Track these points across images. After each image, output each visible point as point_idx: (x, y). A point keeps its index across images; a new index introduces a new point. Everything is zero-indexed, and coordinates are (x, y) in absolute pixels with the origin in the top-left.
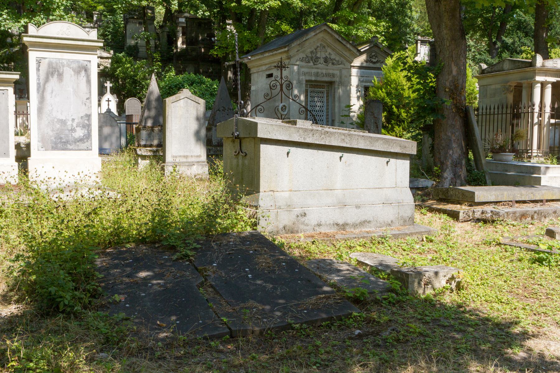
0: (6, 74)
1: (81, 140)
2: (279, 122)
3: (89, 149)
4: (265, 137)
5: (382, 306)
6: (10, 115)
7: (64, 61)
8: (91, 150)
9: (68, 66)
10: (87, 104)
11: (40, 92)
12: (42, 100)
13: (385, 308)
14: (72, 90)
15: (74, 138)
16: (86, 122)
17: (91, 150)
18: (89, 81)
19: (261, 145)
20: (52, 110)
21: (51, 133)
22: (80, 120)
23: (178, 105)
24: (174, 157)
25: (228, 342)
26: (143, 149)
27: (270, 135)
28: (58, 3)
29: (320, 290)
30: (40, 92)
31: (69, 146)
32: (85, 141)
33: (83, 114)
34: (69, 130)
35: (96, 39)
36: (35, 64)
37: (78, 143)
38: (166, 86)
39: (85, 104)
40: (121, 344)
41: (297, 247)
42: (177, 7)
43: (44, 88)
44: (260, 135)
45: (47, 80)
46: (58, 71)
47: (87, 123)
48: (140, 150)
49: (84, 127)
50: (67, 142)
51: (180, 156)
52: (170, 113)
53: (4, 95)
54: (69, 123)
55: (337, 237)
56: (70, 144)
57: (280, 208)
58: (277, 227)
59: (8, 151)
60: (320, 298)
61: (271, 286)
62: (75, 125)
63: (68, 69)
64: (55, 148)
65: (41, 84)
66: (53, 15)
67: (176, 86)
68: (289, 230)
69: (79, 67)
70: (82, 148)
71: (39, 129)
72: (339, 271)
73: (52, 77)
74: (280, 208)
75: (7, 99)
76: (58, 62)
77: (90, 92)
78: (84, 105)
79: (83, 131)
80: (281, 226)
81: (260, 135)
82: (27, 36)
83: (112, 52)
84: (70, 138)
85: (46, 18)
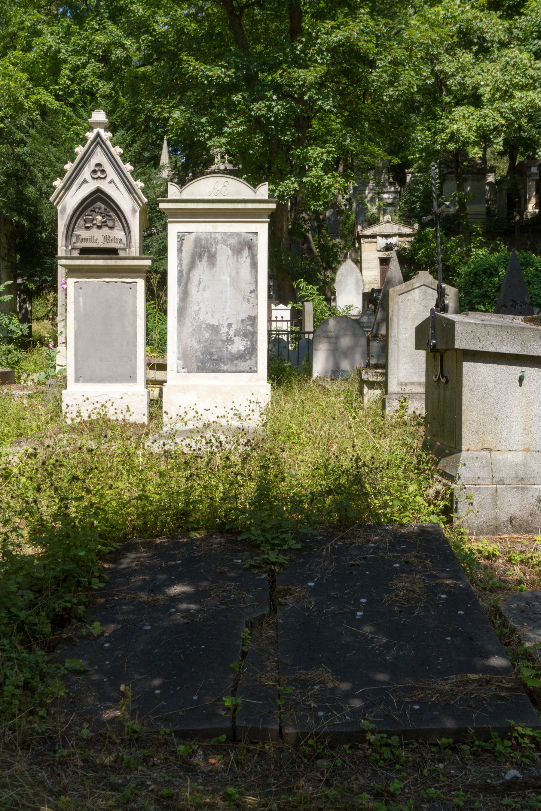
0: (111, 259)
1: (241, 356)
2: (518, 321)
3: (253, 370)
4: (471, 347)
6: (138, 320)
7: (217, 235)
8: (256, 372)
9: (224, 242)
10: (252, 300)
11: (182, 284)
12: (185, 295)
14: (229, 279)
15: (231, 353)
16: (249, 328)
17: (256, 372)
18: (254, 265)
19: (465, 364)
20: (199, 310)
21: (196, 346)
22: (240, 325)
23: (410, 297)
24: (401, 384)
25: (218, 749)
26: (371, 372)
27: (481, 345)
28: (315, 158)
29: (479, 662)
30: (182, 284)
31: (222, 365)
32: (247, 357)
33: (244, 316)
34: (223, 342)
35: (266, 198)
36: (176, 243)
37: (236, 362)
38: (470, 272)
39: (248, 301)
40: (290, 600)
41: (522, 561)
42: (502, 148)
43: (188, 278)
44: (460, 343)
45: (192, 265)
46: (209, 251)
47: (251, 329)
48: (366, 373)
49: (245, 335)
50: (220, 360)
51: (413, 383)
52: (395, 311)
53: (131, 291)
54: (224, 330)
56: (224, 363)
57: (501, 482)
58: (496, 518)
59: (135, 374)
60: (468, 682)
61: (385, 640)
62: (232, 333)
63: (224, 247)
64: (202, 369)
65: (184, 272)
66: (308, 177)
67: (484, 272)
68: (520, 527)
69: (240, 243)
70: (243, 369)
71: (179, 339)
73: (200, 261)
74: (501, 482)
75: (135, 297)
76: (209, 237)
77: (256, 282)
78: (246, 302)
79: (244, 343)
80: (504, 517)
81: (460, 343)
82: (164, 202)
83: (416, 226)
84: (225, 353)
85: (297, 181)
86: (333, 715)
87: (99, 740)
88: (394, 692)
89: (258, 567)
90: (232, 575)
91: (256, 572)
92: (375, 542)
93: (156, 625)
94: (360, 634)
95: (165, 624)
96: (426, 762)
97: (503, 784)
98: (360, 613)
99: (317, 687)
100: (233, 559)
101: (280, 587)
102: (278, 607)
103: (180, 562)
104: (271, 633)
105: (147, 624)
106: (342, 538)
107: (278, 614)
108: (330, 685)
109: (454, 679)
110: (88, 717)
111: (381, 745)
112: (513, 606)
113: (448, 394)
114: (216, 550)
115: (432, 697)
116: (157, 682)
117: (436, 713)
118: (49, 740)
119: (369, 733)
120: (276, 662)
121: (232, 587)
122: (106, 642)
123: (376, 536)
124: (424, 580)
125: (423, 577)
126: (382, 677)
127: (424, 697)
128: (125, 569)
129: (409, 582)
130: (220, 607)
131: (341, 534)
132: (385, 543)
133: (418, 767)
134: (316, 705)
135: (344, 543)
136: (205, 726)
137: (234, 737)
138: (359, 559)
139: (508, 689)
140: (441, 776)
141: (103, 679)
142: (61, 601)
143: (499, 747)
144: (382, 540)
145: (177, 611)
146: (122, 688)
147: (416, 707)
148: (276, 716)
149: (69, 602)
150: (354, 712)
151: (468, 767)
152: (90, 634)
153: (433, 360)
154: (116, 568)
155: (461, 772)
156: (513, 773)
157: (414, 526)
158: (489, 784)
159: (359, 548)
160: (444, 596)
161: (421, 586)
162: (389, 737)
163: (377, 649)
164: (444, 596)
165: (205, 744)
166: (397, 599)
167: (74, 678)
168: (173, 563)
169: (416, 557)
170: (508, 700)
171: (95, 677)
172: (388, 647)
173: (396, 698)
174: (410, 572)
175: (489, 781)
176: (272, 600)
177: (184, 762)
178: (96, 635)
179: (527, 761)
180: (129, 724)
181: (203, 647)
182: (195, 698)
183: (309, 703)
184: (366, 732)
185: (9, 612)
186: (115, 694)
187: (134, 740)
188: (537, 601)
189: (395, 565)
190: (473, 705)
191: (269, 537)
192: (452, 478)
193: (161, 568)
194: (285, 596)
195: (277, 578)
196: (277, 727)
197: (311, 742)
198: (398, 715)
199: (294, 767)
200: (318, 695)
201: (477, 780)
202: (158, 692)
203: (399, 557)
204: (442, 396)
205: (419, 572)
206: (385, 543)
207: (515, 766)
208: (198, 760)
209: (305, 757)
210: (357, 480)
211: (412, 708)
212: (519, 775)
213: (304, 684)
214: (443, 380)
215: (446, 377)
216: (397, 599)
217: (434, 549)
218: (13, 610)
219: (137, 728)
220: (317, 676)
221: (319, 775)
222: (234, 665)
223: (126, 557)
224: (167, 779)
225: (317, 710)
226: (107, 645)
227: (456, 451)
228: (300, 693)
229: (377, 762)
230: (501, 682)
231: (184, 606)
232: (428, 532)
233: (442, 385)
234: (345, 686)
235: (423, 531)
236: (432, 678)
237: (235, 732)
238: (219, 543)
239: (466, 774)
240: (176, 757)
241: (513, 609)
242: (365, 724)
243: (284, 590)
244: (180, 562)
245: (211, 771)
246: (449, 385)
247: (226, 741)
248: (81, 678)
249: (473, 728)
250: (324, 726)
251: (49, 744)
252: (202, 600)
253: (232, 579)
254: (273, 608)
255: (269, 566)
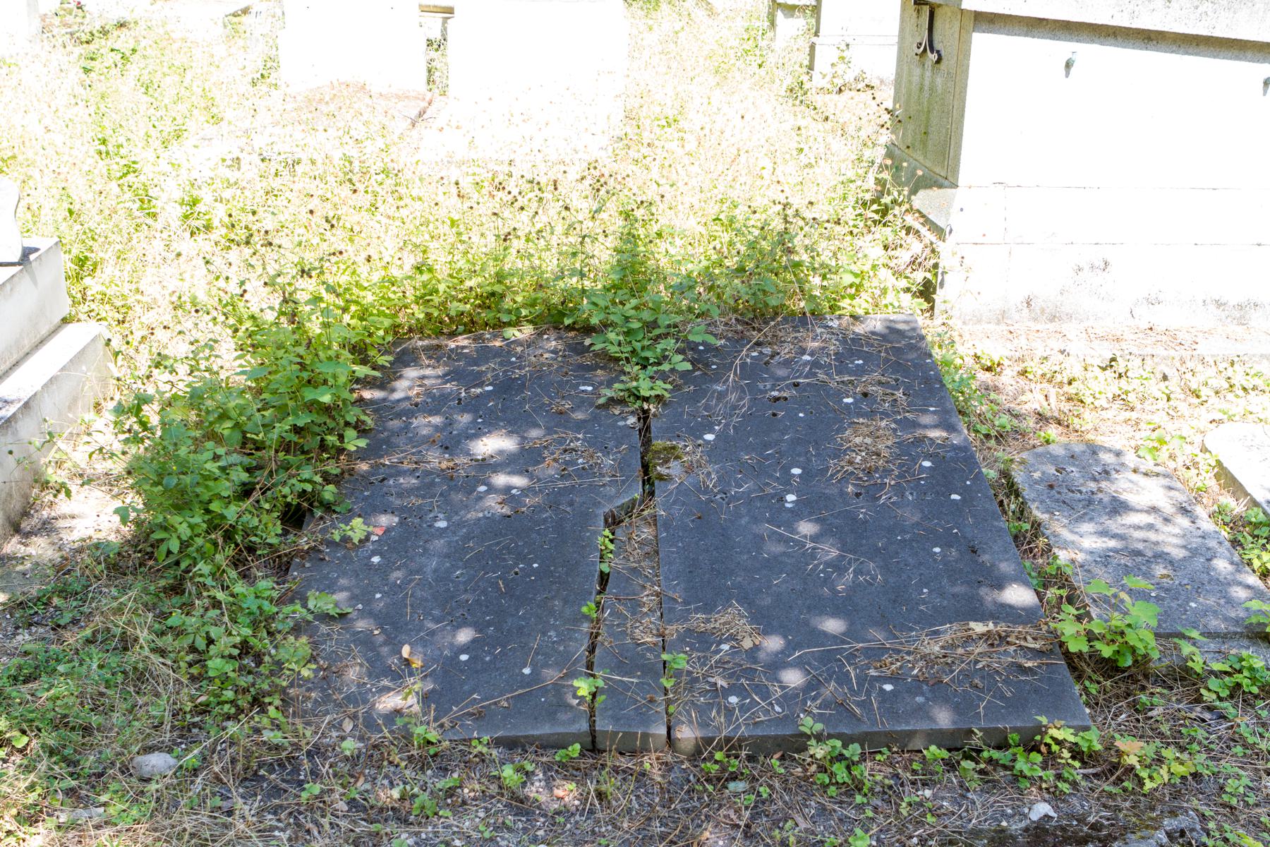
5: (1199, 700)
13: (1210, 709)
25: (568, 770)
29: (989, 596)
40: (674, 469)
55: (1202, 349)
60: (969, 640)
61: (834, 553)
68: (1043, 311)
72: (1118, 507)
86: (753, 702)
87: (373, 758)
88: (851, 657)
89: (621, 402)
90: (579, 416)
91: (617, 412)
92: (812, 354)
93: (456, 518)
94: (793, 540)
95: (472, 515)
96: (902, 785)
97: (1026, 830)
98: (791, 498)
99: (725, 647)
100: (579, 384)
101: (658, 443)
102: (656, 482)
103: (490, 388)
104: (647, 533)
105: (441, 516)
106: (758, 344)
107: (658, 499)
108: (747, 644)
109: (950, 631)
110: (352, 710)
111: (832, 761)
112: (1037, 475)
113: (939, 81)
114: (550, 365)
115: (913, 668)
116: (464, 636)
117: (920, 699)
118: (287, 763)
119: (813, 742)
120: (658, 595)
121: (578, 443)
122: (374, 553)
123: (814, 339)
124: (895, 430)
125: (893, 426)
126: (833, 625)
127: (901, 667)
128: (399, 401)
129: (871, 434)
130: (561, 484)
131: (756, 336)
132: (828, 355)
133: (890, 794)
134: (725, 685)
135: (761, 352)
136: (545, 730)
137: (593, 746)
138: (787, 386)
139: (1039, 653)
140: (929, 816)
141: (372, 631)
142: (294, 481)
143: (1021, 765)
144: (824, 348)
145: (492, 489)
146: (406, 651)
147: (888, 687)
148: (661, 709)
149: (309, 481)
150: (789, 698)
151: (969, 795)
152: (346, 539)
153: (915, 14)
154: (384, 400)
155: (961, 806)
156: (1042, 809)
157: (875, 324)
158: (1003, 831)
159: (787, 363)
160: (927, 464)
161: (889, 443)
162: (845, 746)
163: (822, 571)
164: (927, 464)
165: (544, 759)
166: (850, 468)
167: (324, 629)
168: (479, 390)
169: (880, 383)
170: (1036, 674)
171: (361, 625)
172: (838, 567)
173: (855, 669)
174: (871, 415)
175: (1004, 824)
176: (646, 472)
177: (514, 796)
178: (356, 541)
179: (1064, 787)
180: (420, 730)
181: (535, 565)
182: (527, 671)
183: (713, 680)
184: (809, 737)
185: (208, 511)
186: (393, 661)
187: (431, 760)
188: (1074, 465)
189: (846, 400)
190: (980, 685)
191: (638, 346)
192: (939, 232)
193: (460, 400)
194: (666, 461)
195: (654, 424)
196: (663, 731)
197: (719, 756)
198: (858, 704)
199: (692, 799)
200: (728, 662)
201: (986, 821)
202: (464, 657)
203: (851, 382)
204: (927, 83)
205: (885, 415)
206: (828, 355)
207: (1047, 796)
208: (536, 790)
209: (709, 780)
210: (784, 241)
211: (882, 690)
212: (1052, 813)
213: (703, 641)
214: (934, 57)
215: (938, 52)
216: (850, 468)
217: (904, 363)
218: (215, 506)
219: (433, 736)
220: (724, 624)
221: (731, 813)
222: (588, 608)
223: (401, 377)
224: (487, 835)
225: (726, 692)
226: (376, 559)
227: (946, 183)
228: (699, 658)
229: (825, 787)
230: (1025, 639)
231: (501, 480)
232: (898, 332)
233: (929, 64)
234: (774, 643)
235: (892, 333)
236: (912, 629)
237: (594, 737)
238: (555, 352)
239: (967, 810)
240: (500, 787)
241: (1036, 482)
242: (808, 724)
243: (665, 449)
244: (490, 388)
245: (558, 813)
246: (943, 65)
247: (582, 755)
248: (337, 627)
249: (980, 730)
250: (739, 727)
251: (289, 768)
252: (530, 469)
253: (579, 426)
254: (649, 480)
255: (639, 403)
